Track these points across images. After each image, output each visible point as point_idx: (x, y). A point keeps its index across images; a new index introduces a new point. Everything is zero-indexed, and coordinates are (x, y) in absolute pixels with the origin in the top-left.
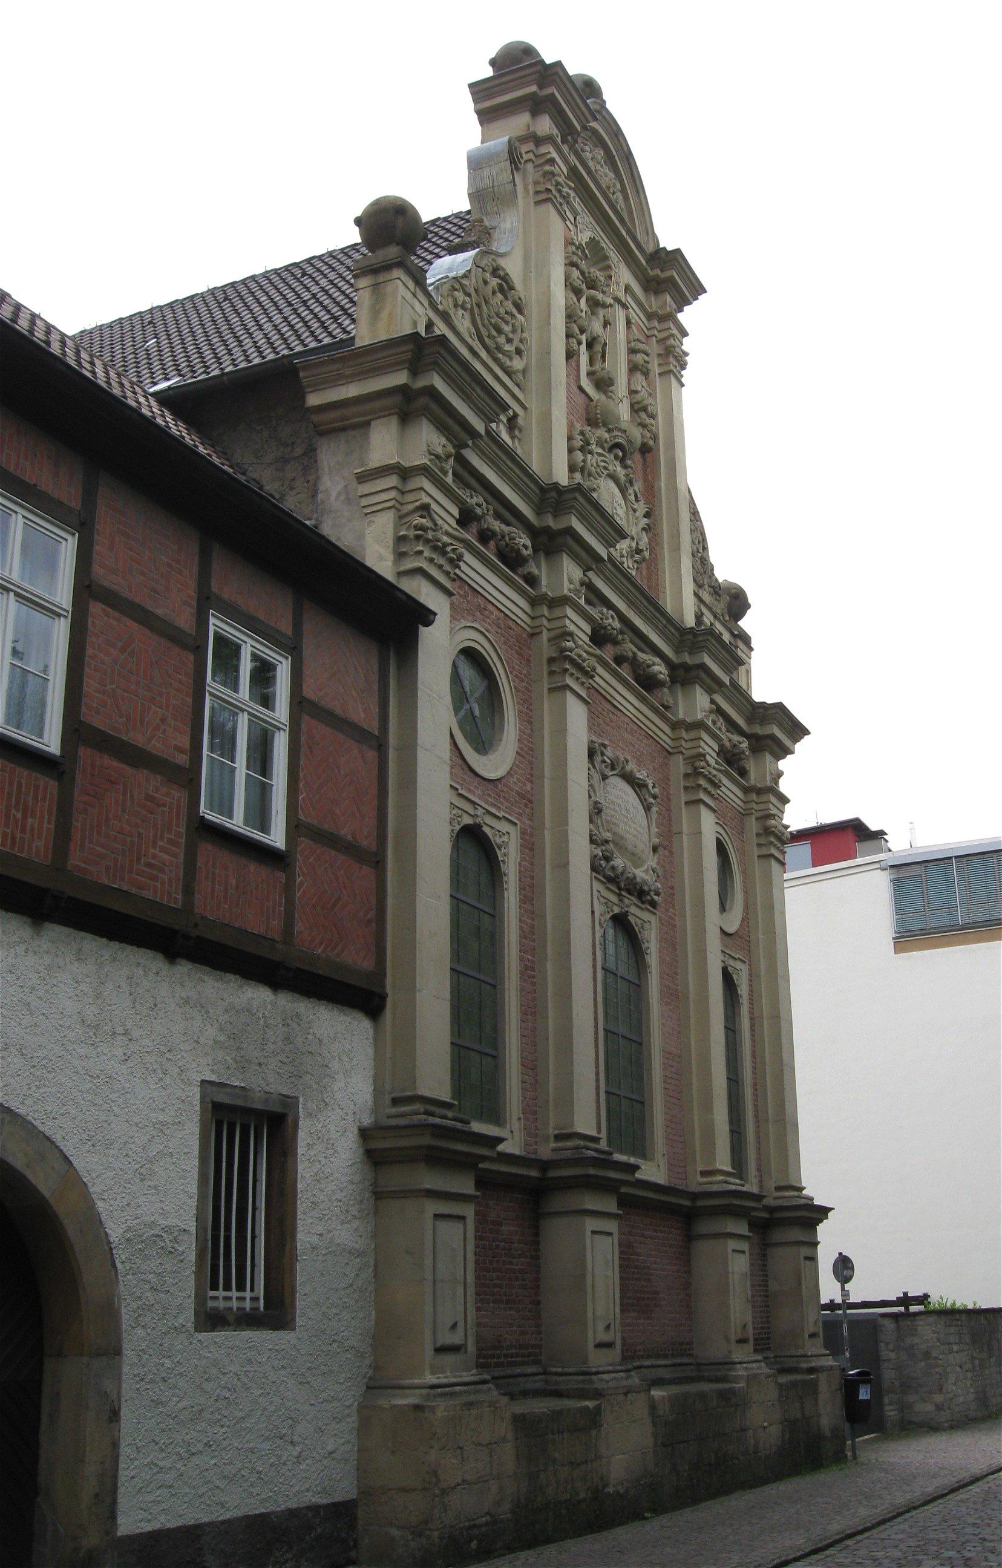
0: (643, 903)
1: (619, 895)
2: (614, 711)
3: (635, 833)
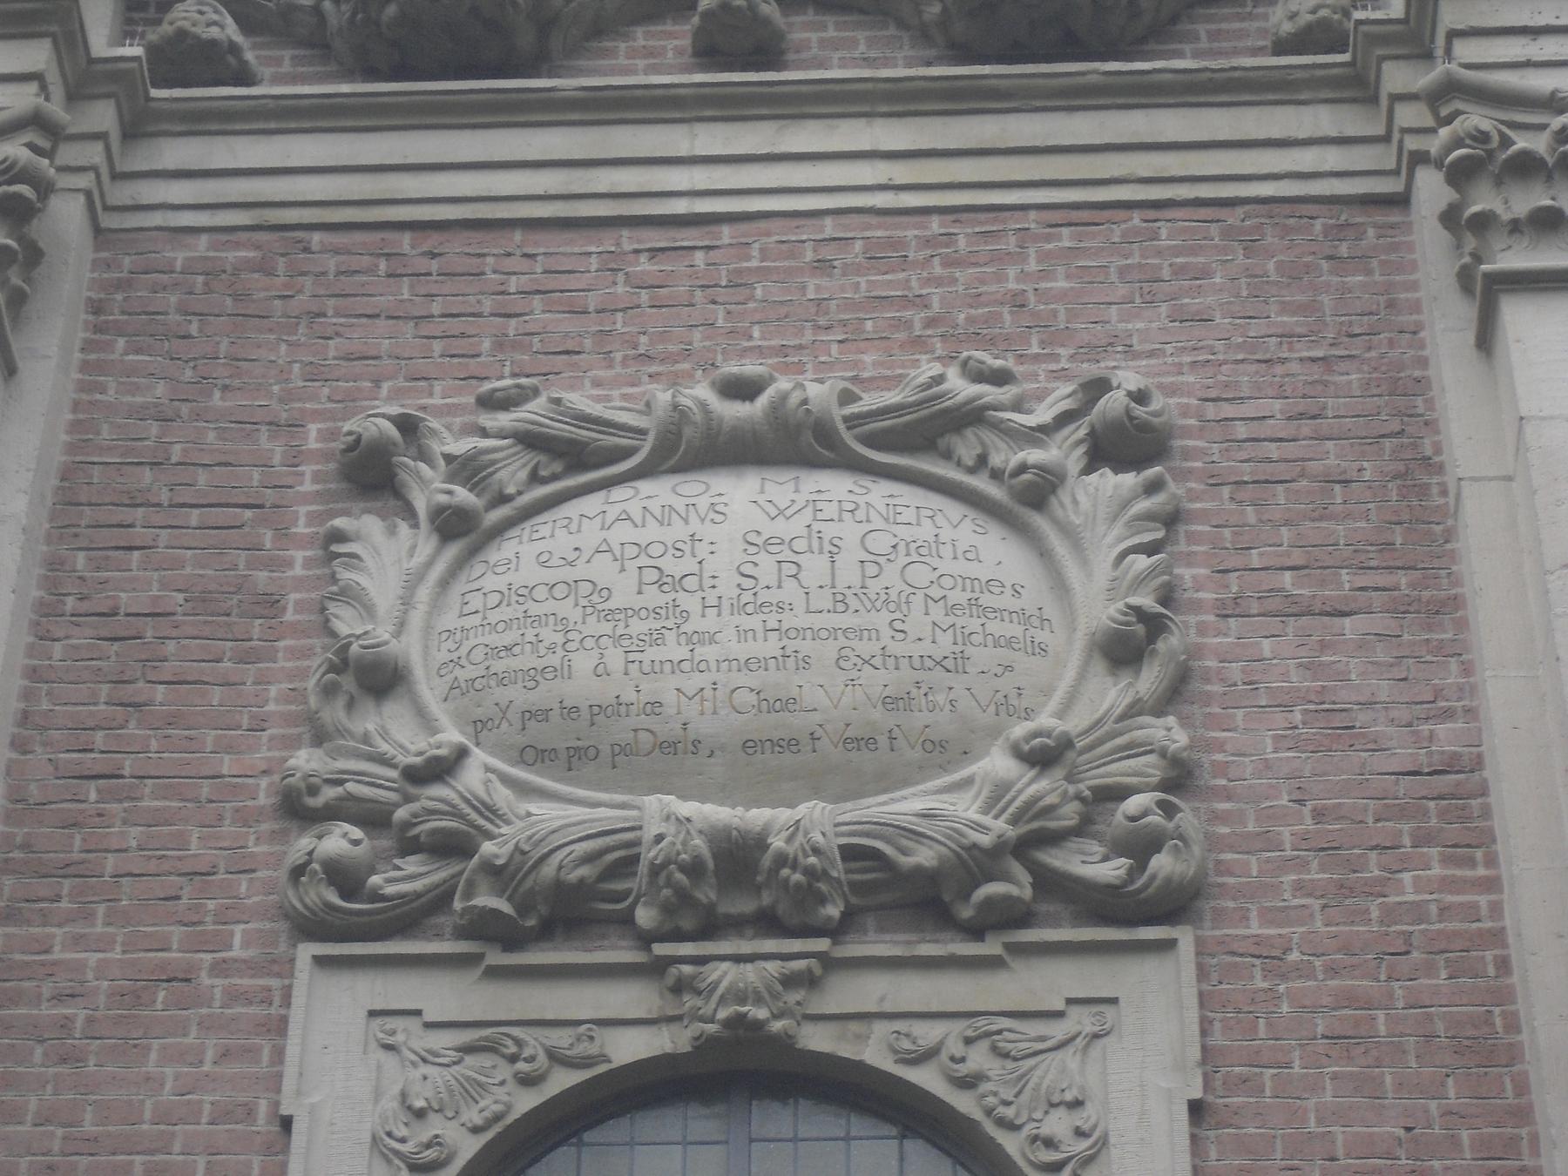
0: (976, 932)
1: (656, 969)
2: (687, 237)
3: (772, 646)
